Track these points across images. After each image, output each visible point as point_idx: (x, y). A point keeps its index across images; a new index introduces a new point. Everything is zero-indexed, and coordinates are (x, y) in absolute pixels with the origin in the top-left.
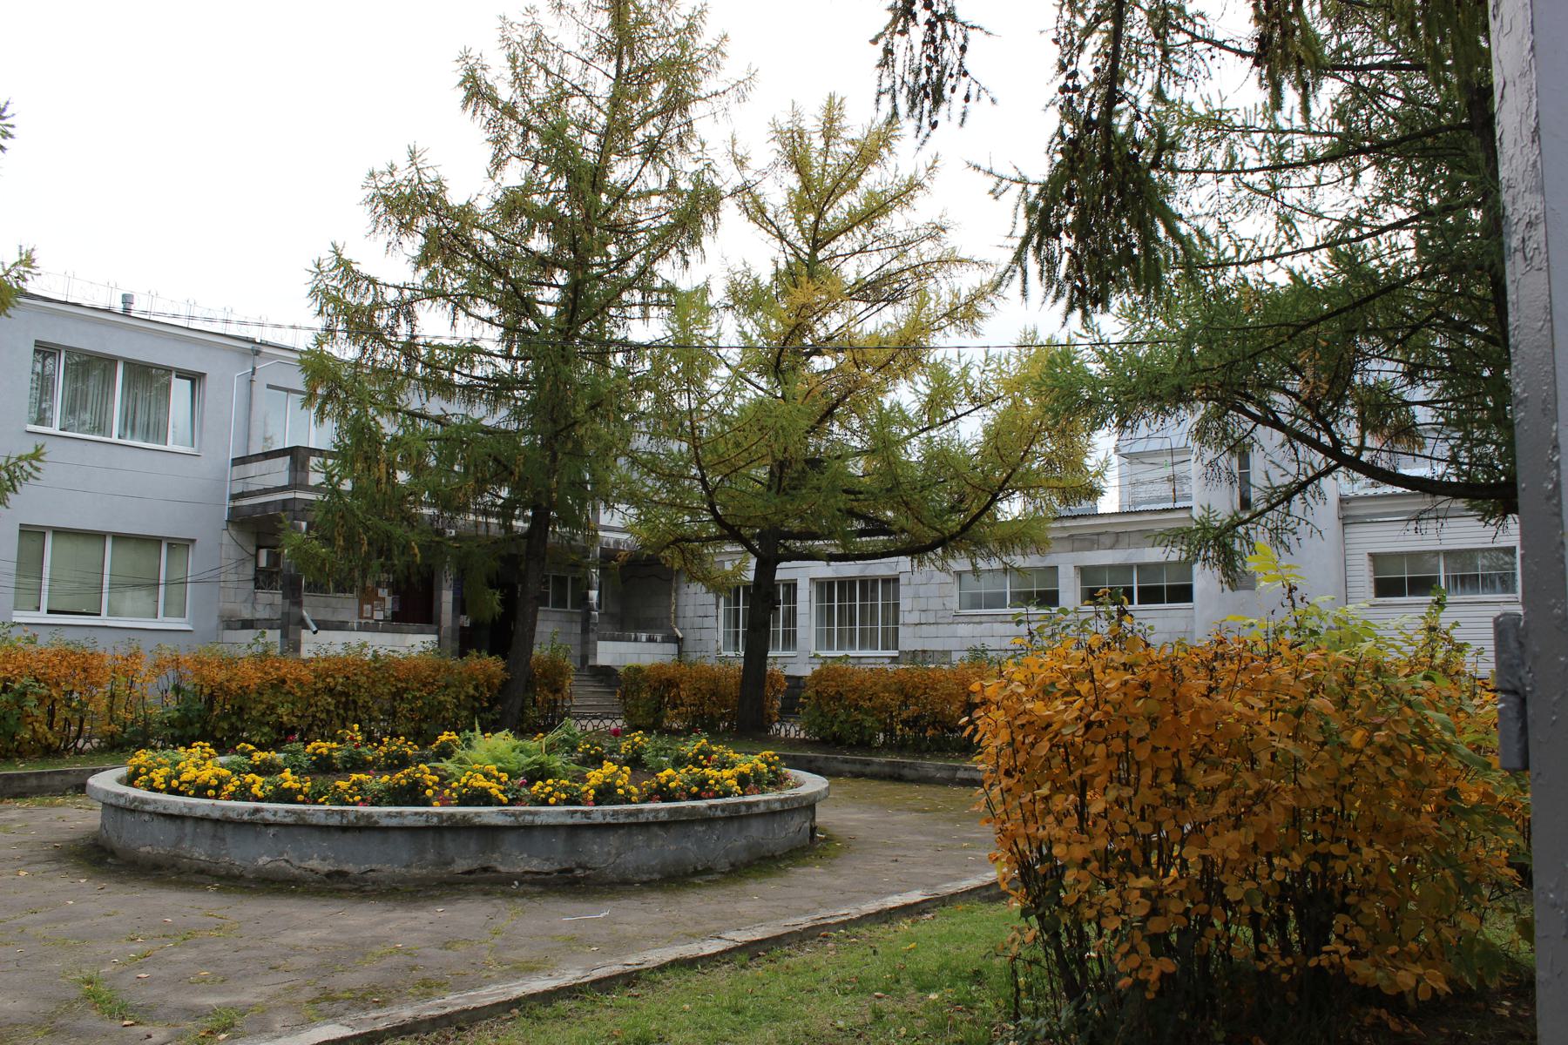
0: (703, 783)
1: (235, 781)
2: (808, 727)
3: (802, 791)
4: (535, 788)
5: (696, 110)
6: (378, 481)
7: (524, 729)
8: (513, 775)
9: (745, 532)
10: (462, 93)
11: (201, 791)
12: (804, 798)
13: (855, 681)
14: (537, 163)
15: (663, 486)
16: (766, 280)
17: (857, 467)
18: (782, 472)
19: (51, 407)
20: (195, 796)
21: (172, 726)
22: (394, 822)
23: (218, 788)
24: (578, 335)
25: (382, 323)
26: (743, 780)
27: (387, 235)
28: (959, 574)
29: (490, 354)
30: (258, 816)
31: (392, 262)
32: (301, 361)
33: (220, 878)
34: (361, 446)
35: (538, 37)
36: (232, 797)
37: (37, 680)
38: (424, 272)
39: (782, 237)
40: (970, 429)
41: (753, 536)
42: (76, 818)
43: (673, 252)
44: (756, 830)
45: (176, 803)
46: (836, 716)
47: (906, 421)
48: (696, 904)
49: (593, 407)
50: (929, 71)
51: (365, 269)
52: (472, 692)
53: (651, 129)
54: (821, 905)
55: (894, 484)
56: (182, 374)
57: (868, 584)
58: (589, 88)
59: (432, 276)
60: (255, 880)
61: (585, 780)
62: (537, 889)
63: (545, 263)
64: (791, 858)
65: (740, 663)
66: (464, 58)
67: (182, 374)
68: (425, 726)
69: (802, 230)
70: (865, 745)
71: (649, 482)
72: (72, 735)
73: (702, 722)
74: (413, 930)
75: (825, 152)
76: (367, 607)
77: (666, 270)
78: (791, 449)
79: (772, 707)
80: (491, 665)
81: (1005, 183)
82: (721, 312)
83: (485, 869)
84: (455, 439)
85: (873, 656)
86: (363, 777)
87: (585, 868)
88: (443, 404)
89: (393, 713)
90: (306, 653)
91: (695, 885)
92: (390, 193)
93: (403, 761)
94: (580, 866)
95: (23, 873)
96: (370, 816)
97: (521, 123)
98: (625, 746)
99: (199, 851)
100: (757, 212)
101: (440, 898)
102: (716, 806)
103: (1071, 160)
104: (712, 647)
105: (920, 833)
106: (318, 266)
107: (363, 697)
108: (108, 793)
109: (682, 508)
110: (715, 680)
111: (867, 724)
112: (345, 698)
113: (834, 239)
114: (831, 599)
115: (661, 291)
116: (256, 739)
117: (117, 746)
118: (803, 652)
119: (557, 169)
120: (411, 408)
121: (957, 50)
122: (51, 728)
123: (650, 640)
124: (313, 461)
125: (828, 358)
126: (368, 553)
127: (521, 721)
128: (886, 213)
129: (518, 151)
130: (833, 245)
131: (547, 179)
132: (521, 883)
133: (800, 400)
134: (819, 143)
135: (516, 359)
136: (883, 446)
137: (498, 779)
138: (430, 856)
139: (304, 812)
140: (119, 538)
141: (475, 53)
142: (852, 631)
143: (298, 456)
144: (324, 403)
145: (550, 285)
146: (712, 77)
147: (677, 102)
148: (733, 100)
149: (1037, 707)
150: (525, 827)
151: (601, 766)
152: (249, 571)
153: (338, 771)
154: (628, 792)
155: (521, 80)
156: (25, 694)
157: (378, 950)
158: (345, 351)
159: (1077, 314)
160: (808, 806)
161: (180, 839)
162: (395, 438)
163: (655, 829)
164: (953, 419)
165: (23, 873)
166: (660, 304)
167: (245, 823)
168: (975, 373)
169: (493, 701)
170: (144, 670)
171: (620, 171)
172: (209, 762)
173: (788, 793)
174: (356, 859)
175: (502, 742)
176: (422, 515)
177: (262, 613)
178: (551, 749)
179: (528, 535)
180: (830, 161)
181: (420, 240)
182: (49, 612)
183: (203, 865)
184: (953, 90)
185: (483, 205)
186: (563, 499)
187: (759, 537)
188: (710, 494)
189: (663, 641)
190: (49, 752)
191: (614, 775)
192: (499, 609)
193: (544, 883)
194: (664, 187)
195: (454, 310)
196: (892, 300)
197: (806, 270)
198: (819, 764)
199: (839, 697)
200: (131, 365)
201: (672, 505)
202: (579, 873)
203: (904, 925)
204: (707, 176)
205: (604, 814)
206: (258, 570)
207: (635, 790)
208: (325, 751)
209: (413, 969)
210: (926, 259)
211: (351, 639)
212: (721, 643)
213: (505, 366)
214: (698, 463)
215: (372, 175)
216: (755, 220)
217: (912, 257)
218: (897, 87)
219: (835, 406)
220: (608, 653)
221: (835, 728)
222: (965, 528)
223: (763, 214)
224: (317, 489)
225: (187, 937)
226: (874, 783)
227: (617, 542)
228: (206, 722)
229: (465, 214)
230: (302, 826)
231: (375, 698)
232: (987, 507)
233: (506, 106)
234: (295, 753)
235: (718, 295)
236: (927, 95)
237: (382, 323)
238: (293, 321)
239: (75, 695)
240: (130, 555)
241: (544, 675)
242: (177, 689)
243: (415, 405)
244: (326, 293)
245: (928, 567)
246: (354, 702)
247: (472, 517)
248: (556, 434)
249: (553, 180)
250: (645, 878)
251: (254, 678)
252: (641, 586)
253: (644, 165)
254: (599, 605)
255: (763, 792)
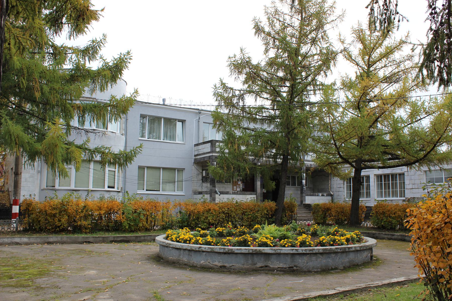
0: (334, 241)
1: (194, 239)
2: (374, 223)
3: (367, 244)
4: (281, 242)
5: (326, 27)
6: (235, 150)
7: (280, 224)
8: (274, 238)
9: (350, 160)
10: (254, 30)
11: (185, 242)
12: (367, 246)
13: (389, 208)
14: (278, 49)
15: (323, 147)
16: (354, 79)
17: (388, 137)
18: (361, 140)
19: (145, 133)
20: (183, 243)
21: (179, 223)
22: (239, 252)
23: (190, 241)
24: (294, 101)
25: (235, 102)
26: (347, 240)
27: (235, 75)
28: (425, 172)
29: (268, 109)
30: (201, 249)
31: (237, 83)
32: (212, 115)
33: (190, 267)
34: (230, 139)
35: (276, 11)
36: (194, 243)
37: (143, 210)
38: (246, 86)
39: (358, 65)
40: (426, 123)
41: (353, 162)
42: (153, 249)
43: (322, 72)
44: (352, 256)
45: (178, 245)
46: (382, 219)
47: (403, 121)
48: (331, 279)
49: (300, 123)
50: (386, 14)
51: (229, 85)
52: (266, 212)
53: (313, 35)
54: (372, 281)
55: (399, 143)
56: (179, 121)
57: (394, 176)
58: (293, 24)
59: (249, 87)
60: (200, 267)
61: (297, 240)
62: (282, 273)
63: (283, 80)
64: (364, 265)
65: (351, 202)
66: (254, 20)
67: (179, 121)
68: (252, 223)
69: (364, 62)
70: (393, 229)
71: (319, 146)
72: (153, 225)
73: (339, 223)
74: (244, 284)
75: (370, 36)
76: (235, 187)
77: (320, 79)
78: (364, 133)
79: (361, 217)
80: (272, 204)
81: (416, 46)
82: (339, 90)
83: (266, 266)
84: (258, 135)
85: (397, 200)
86: (230, 238)
87: (297, 267)
88: (254, 125)
89: (242, 219)
90: (217, 201)
91: (331, 273)
92: (235, 63)
93: (244, 233)
94: (295, 266)
95: (140, 263)
96: (232, 250)
97: (272, 37)
98: (312, 229)
99: (185, 258)
100: (349, 57)
101: (253, 274)
102: (338, 248)
103: (435, 37)
104: (343, 197)
105: (410, 259)
106: (215, 86)
107: (233, 214)
108: (160, 242)
109: (329, 153)
110: (343, 208)
111: (393, 222)
112: (228, 215)
113: (375, 63)
114: (381, 181)
115: (319, 85)
116: (203, 227)
117: (164, 228)
118: (372, 198)
119: (285, 50)
120: (245, 127)
121: (395, 6)
122: (147, 223)
123: (323, 195)
124: (217, 144)
125: (375, 103)
126: (233, 171)
127: (281, 221)
128: (392, 53)
129: (272, 46)
130: (374, 66)
131: (282, 54)
132: (277, 271)
133: (365, 117)
134: (368, 33)
135: (276, 110)
136: (395, 131)
137: (270, 239)
138: (250, 262)
139: (213, 248)
140: (164, 169)
141: (257, 18)
142: (389, 192)
143: (213, 143)
144: (219, 127)
145: (285, 86)
146: (332, 16)
147: (320, 26)
148: (339, 21)
149: (429, 216)
150: (278, 254)
151: (302, 235)
152: (200, 177)
153: (225, 236)
154: (310, 243)
155: (272, 25)
156: (140, 214)
157: (233, 289)
158: (225, 111)
159: (442, 86)
160: (370, 249)
161: (180, 255)
162: (240, 137)
163: (319, 255)
164: (419, 120)
165: (140, 263)
166: (319, 89)
167: (197, 251)
168: (426, 104)
169: (273, 215)
170: (171, 207)
171: (304, 49)
172: (188, 233)
173: (362, 244)
174: (228, 262)
175: (273, 228)
176: (249, 159)
177: (204, 190)
178: (288, 230)
179: (282, 164)
180: (372, 38)
181: (244, 76)
182: (147, 190)
183: (186, 263)
184: (394, 19)
185: (263, 64)
186: (292, 152)
187: (355, 161)
188: (338, 149)
189: (327, 196)
190: (147, 230)
191: (306, 238)
192: (274, 187)
193: (283, 271)
194: (318, 52)
195: (256, 96)
196: (396, 82)
197: (367, 74)
198: (377, 235)
199: (384, 213)
200: (165, 119)
201: (326, 153)
202: (295, 268)
203: (397, 288)
204: (331, 47)
205: (302, 250)
206: (203, 177)
207: (312, 243)
208: (221, 230)
209: (243, 295)
210: (407, 67)
211: (232, 197)
212: (345, 196)
213: (272, 112)
214: (333, 139)
215: (230, 58)
216: (349, 60)
217: (402, 67)
218: (376, 21)
219: (378, 118)
220: (309, 200)
221: (382, 224)
222: (425, 156)
223: (351, 58)
224: (218, 152)
225: (181, 283)
226: (395, 242)
227: (311, 165)
228: (188, 222)
229: (257, 67)
230: (212, 252)
231: (237, 215)
232: (433, 148)
233: (268, 32)
234: (212, 231)
235: (339, 84)
236: (385, 22)
237: (235, 102)
238: (209, 103)
239: (153, 214)
240: (167, 173)
241: (288, 207)
242: (180, 212)
243: (246, 126)
244: (218, 93)
245: (413, 170)
246: (231, 216)
247: (264, 159)
248: (289, 133)
249: (283, 54)
250: (316, 270)
251: (201, 209)
252: (319, 178)
253: (311, 46)
254: (306, 185)
255: (354, 244)
